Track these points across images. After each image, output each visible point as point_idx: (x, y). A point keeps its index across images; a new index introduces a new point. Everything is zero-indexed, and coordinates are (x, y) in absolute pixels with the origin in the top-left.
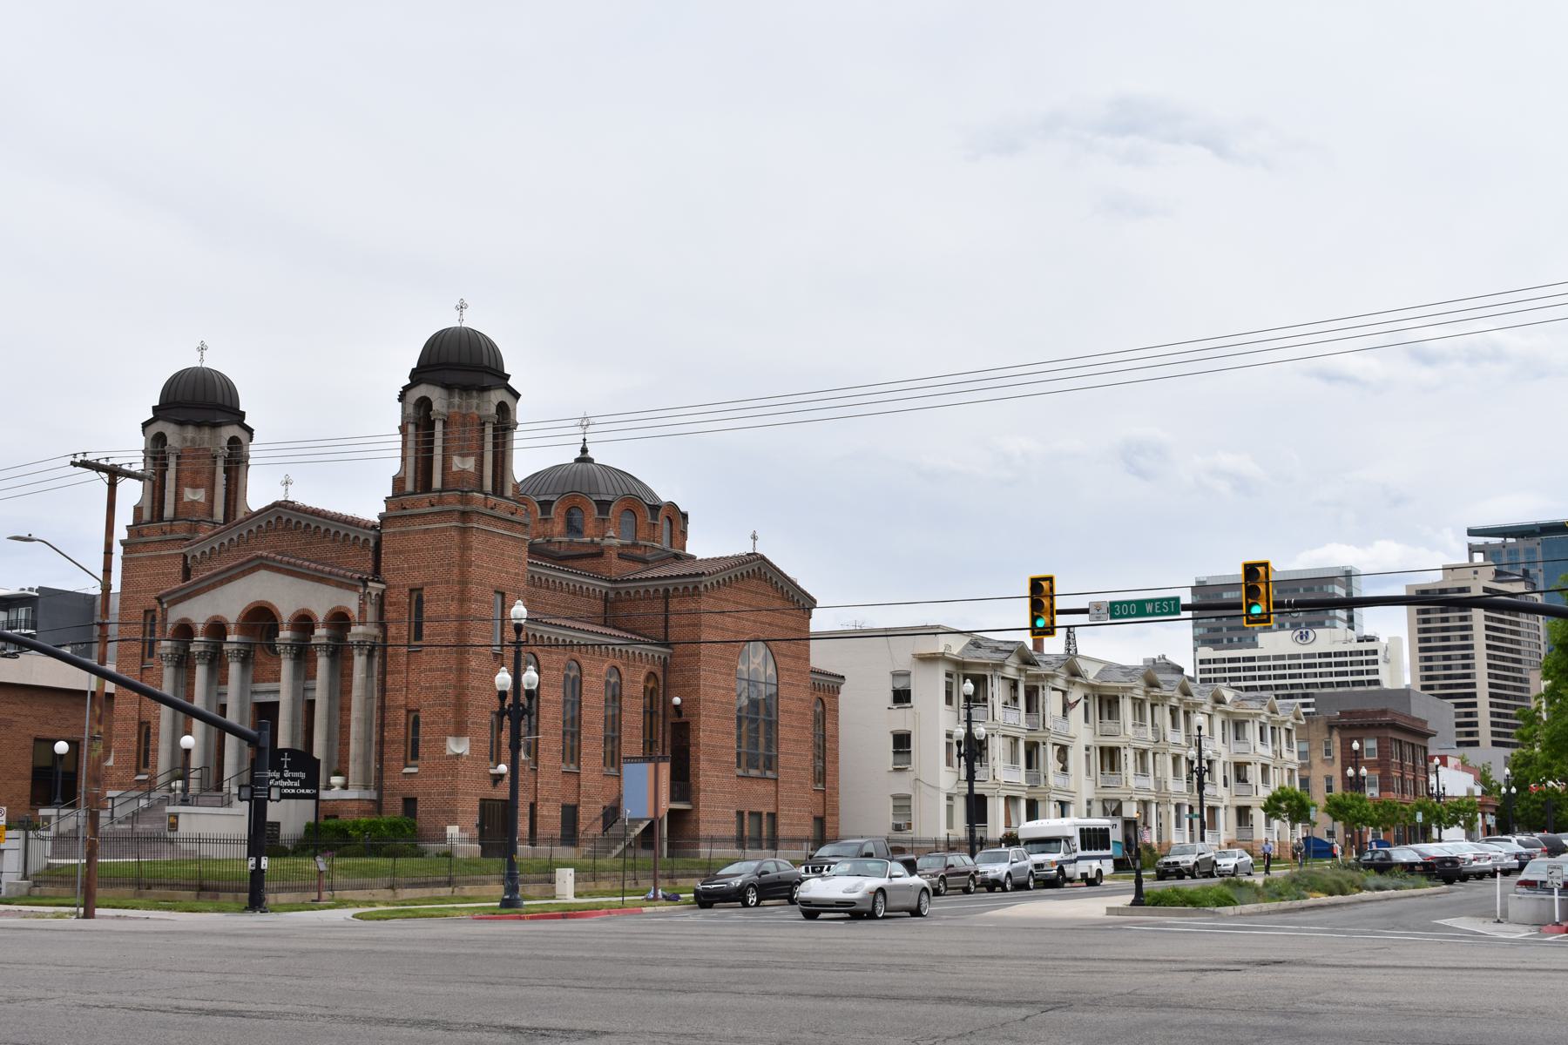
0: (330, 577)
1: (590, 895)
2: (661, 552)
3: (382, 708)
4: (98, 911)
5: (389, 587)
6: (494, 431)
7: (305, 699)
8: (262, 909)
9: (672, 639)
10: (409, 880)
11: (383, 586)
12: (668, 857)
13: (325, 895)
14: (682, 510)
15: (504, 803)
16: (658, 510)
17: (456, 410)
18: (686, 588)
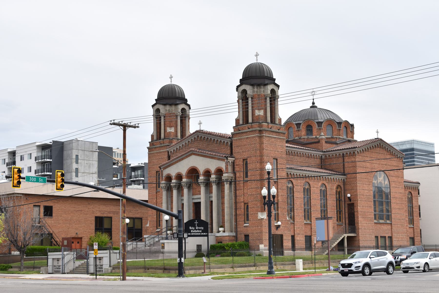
0: (215, 156)
1: (309, 269)
2: (343, 140)
3: (236, 203)
4: (127, 278)
5: (236, 159)
6: (270, 99)
7: (210, 200)
8: (183, 276)
9: (346, 172)
10: (239, 265)
11: (234, 159)
12: (348, 254)
13: (207, 271)
14: (350, 123)
15: (281, 236)
16: (341, 124)
17: (256, 93)
18: (350, 153)
